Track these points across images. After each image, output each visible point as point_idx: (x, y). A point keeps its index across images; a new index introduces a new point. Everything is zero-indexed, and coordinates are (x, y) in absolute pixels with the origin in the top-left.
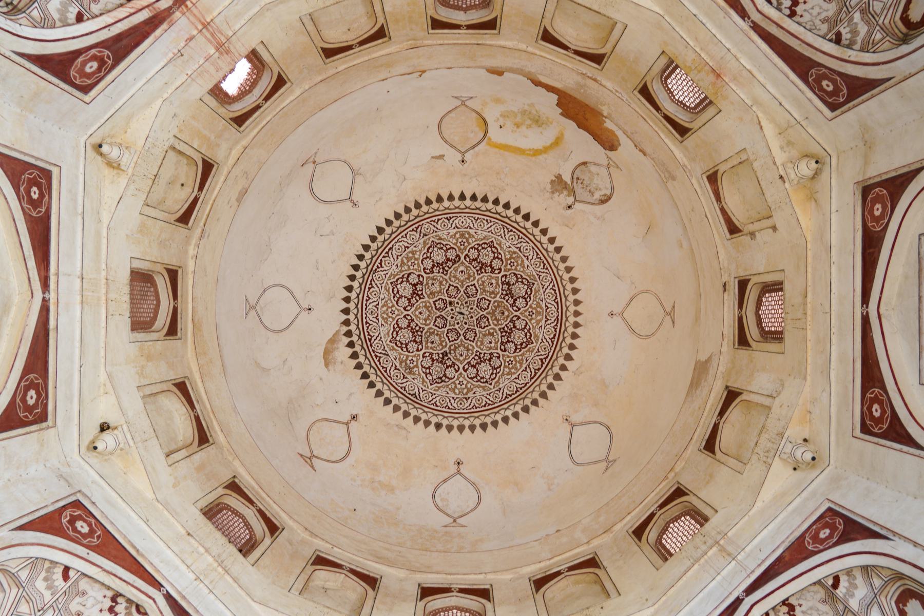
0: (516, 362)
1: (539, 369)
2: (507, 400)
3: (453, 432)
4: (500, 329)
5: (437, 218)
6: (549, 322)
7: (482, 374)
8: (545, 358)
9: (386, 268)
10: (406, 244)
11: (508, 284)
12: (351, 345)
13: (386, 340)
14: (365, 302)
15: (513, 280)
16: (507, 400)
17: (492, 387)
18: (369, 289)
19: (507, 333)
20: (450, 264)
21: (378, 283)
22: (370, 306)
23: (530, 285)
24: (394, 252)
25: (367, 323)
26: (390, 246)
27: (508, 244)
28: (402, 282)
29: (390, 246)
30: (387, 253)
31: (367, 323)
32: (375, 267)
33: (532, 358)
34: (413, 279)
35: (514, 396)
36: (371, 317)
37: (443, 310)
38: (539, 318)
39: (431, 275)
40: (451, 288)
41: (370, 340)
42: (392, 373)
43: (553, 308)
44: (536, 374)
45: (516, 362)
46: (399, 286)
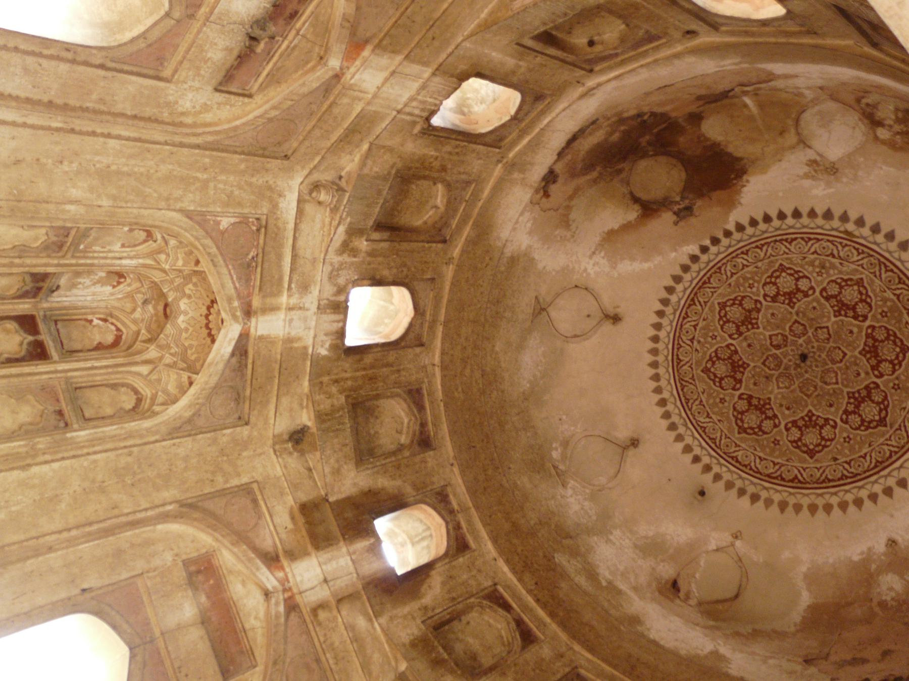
1: (783, 479)
2: (730, 460)
4: (848, 393)
5: (892, 267)
6: (846, 466)
7: (746, 418)
8: (800, 482)
9: (792, 249)
10: (835, 252)
11: (869, 395)
12: (694, 258)
14: (739, 252)
15: (877, 398)
16: (730, 460)
17: (737, 435)
19: (810, 421)
20: (851, 313)
21: (702, 300)
22: (739, 260)
24: (816, 245)
25: (720, 268)
26: (820, 237)
29: (820, 237)
30: (810, 239)
31: (720, 268)
32: (785, 237)
33: (798, 464)
35: (737, 465)
36: (729, 268)
37: (795, 336)
39: (822, 300)
41: (705, 283)
42: (687, 326)
43: (866, 465)
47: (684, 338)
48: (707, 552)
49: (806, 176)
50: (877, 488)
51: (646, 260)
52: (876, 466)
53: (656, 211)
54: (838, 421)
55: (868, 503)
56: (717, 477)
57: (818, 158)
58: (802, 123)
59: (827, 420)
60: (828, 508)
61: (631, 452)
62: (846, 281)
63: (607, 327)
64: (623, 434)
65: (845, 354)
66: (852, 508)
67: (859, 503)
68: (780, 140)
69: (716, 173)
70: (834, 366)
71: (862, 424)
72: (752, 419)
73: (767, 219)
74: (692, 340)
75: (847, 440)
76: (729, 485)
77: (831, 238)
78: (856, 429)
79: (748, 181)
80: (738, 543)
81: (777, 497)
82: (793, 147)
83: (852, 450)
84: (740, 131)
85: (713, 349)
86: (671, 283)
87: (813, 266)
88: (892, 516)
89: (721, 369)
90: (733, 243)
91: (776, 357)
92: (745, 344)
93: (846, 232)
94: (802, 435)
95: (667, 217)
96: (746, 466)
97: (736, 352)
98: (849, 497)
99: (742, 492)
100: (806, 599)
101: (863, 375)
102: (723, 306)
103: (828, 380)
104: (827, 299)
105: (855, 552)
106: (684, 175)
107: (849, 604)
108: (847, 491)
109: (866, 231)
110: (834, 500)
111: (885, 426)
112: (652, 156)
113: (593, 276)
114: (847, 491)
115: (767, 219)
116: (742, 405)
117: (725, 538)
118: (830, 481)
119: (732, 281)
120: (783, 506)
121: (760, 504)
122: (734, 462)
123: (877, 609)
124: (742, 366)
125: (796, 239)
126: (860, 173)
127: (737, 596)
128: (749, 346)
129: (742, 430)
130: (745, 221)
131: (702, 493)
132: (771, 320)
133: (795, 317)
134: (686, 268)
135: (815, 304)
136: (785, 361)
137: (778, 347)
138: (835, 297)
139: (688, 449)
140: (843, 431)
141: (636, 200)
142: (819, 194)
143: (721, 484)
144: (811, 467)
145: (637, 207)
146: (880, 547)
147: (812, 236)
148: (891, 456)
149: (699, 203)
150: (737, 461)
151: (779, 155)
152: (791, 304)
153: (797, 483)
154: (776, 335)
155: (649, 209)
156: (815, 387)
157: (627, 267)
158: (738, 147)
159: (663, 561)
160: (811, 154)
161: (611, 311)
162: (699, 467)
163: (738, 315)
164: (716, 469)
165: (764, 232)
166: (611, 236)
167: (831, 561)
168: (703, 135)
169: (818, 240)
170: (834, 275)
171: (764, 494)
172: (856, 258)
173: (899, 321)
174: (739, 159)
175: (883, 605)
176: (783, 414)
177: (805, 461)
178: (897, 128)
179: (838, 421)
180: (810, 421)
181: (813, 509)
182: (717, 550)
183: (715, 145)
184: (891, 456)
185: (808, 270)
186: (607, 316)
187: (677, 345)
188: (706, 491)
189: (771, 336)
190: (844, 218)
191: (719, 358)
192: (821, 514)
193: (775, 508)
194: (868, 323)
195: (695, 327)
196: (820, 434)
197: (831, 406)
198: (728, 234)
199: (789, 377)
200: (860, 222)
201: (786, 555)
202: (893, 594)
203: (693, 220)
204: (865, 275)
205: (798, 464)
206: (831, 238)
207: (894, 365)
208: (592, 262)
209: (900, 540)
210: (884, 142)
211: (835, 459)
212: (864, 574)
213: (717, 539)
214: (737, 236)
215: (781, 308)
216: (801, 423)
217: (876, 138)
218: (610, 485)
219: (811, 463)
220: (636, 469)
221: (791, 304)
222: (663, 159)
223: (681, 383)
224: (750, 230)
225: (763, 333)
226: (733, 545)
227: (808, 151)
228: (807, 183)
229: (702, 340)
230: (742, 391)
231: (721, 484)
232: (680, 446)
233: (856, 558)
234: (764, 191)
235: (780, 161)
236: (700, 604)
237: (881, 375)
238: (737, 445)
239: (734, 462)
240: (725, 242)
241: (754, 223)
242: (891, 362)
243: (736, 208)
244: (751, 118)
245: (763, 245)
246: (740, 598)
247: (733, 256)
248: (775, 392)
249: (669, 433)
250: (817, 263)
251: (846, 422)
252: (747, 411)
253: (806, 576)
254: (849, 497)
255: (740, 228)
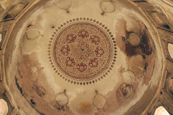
0: (91, 32)
1: (56, 45)
3: (111, 32)
8: (55, 48)
12: (112, 36)
13: (105, 53)
18: (110, 50)
20: (91, 62)
23: (67, 65)
25: (108, 40)
27: (77, 73)
28: (102, 54)
30: (108, 61)
31: (108, 40)
32: (110, 56)
33: (59, 48)
34: (99, 55)
38: (94, 32)
40: (88, 56)
41: (105, 36)
44: (56, 43)
45: (91, 32)
46: (102, 52)
47: (93, 27)
48: (38, 30)
49: (122, 66)
50: (54, 64)
51: (115, 26)
52: (58, 64)
53: (127, 34)
54: (68, 56)
55: (51, 62)
56: (57, 30)
57: (124, 71)
58: (133, 73)
59: (68, 54)
60: (49, 55)
61: (65, 11)
62: (98, 64)
63: (101, 12)
64: (71, 10)
65: (82, 59)
66: (49, 59)
67: (51, 61)
68: (131, 66)
69: (130, 51)
70: (80, 56)
71: (67, 61)
72: (70, 38)
73: (115, 54)
74: (92, 29)
75: (64, 58)
76: (55, 33)
77: (107, 65)
78: (66, 60)
79: (125, 55)
80: (41, 36)
81: (51, 44)
82: (128, 68)
83: (62, 59)
84: (137, 61)
85: (89, 33)
86: (108, 29)
87: (102, 59)
88: (48, 68)
89: (83, 33)
90: (113, 57)
91: (84, 44)
92: (88, 39)
93: (107, 68)
94: (66, 48)
95: (124, 35)
96: (59, 36)
97: (87, 37)
98: (52, 59)
99: (53, 36)
100: (29, 53)
101: (77, 62)
102: (99, 38)
103: (77, 54)
104: (95, 59)
105: (40, 61)
106: (133, 45)
107: (30, 63)
108: (53, 58)
109: (107, 72)
110: (51, 56)
111: (66, 66)
112: (140, 43)
113: (116, 14)
114: (53, 58)
115: (115, 54)
116: (74, 36)
117: (42, 33)
118: (55, 55)
119: (104, 41)
120: (50, 45)
121: (50, 40)
122: (60, 34)
123: (29, 69)
124: (83, 37)
125: (109, 58)
126: (118, 76)
127: (28, 39)
128: (88, 40)
129: (68, 36)
130: (116, 50)
131: (53, 27)
132: (93, 47)
133: (92, 51)
134: (110, 33)
135: (94, 56)
136: (83, 46)
137: (86, 45)
138: (95, 60)
139: (65, 24)
140: (66, 57)
141: (131, 32)
142: (117, 67)
143: (55, 31)
144: (58, 51)
145: (129, 31)
146: (42, 66)
147: (109, 61)
148: (60, 67)
149: (124, 43)
150: (61, 35)
151: (128, 64)
152: (95, 51)
153: (55, 48)
154: (89, 46)
155: (128, 33)
156: (76, 51)
157: (116, 22)
158: (133, 58)
159: (36, 21)
160: (126, 70)
161: (105, 14)
162: (60, 26)
163: (95, 40)
164: (59, 30)
165: (113, 53)
166: (125, 23)
167: (38, 57)
168: (139, 54)
169: (108, 62)
170: (99, 62)
171: (52, 41)
172: (102, 67)
173: (87, 72)
174: (131, 57)
175: (31, 69)
176: (71, 44)
177: (60, 49)
178: (124, 88)
179: (68, 56)
180: (68, 50)
181: (49, 51)
182: (39, 32)
183: (136, 55)
184: (60, 67)
185: (102, 57)
186: (104, 12)
187: (92, 25)
188: (66, 90)
189: (89, 45)
190: (110, 69)
191: (86, 33)
192: (48, 53)
193: (49, 43)
194: (88, 65)
195: (95, 30)
196: (66, 52)
197: (71, 55)
198: (115, 45)
199: (79, 46)
200: (109, 71)
201: (39, 47)
202: (33, 71)
203: (121, 40)
204: (98, 68)
205: (59, 48)
206: (107, 65)
207: (78, 69)
208: (120, 15)
209: (43, 70)
210: (123, 84)
211: (60, 55)
212: (36, 64)
213: (42, 32)
214: (114, 47)
215: (95, 49)
216: (68, 48)
217: (124, 84)
218: (57, 7)
219: (59, 50)
220: (61, 13)
221: (95, 51)
222: (138, 44)
223: (82, 24)
224: (114, 50)
225: (90, 44)
226: (40, 35)
227: (126, 70)
228: (120, 66)
229: (92, 31)
230: (77, 36)
231: (55, 31)
232: (66, 22)
233: (39, 62)
234: (122, 57)
235: (127, 64)
236: (26, 33)
237: (77, 66)
238: (64, 35)
239: (60, 34)
240: (114, 44)
241: (116, 51)
242: (79, 68)
243: (120, 50)
244: (138, 65)
245: (110, 51)
246: (28, 40)
247: (109, 44)
248: (76, 43)
249: (69, 20)
250: (103, 60)
251: (68, 58)
252: (72, 37)
253: (34, 52)
254: (52, 59)
255: (115, 48)
